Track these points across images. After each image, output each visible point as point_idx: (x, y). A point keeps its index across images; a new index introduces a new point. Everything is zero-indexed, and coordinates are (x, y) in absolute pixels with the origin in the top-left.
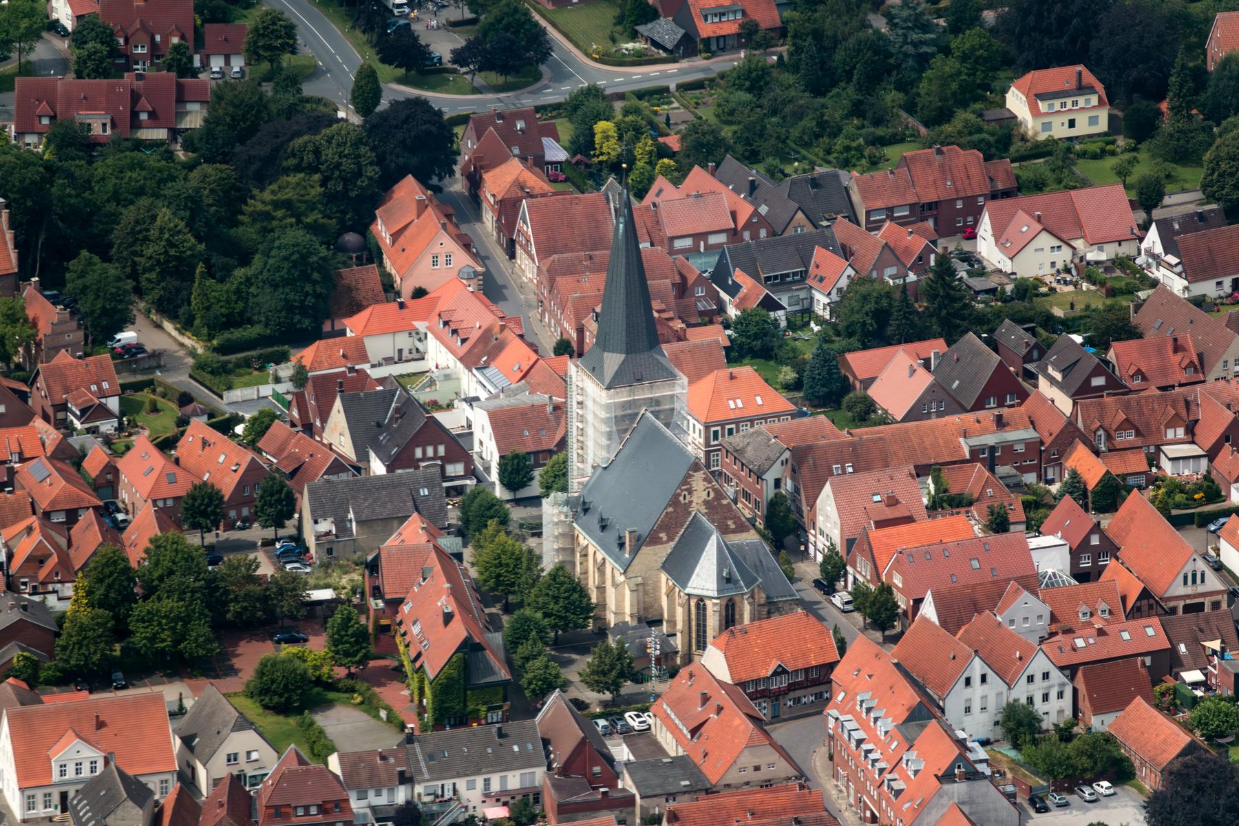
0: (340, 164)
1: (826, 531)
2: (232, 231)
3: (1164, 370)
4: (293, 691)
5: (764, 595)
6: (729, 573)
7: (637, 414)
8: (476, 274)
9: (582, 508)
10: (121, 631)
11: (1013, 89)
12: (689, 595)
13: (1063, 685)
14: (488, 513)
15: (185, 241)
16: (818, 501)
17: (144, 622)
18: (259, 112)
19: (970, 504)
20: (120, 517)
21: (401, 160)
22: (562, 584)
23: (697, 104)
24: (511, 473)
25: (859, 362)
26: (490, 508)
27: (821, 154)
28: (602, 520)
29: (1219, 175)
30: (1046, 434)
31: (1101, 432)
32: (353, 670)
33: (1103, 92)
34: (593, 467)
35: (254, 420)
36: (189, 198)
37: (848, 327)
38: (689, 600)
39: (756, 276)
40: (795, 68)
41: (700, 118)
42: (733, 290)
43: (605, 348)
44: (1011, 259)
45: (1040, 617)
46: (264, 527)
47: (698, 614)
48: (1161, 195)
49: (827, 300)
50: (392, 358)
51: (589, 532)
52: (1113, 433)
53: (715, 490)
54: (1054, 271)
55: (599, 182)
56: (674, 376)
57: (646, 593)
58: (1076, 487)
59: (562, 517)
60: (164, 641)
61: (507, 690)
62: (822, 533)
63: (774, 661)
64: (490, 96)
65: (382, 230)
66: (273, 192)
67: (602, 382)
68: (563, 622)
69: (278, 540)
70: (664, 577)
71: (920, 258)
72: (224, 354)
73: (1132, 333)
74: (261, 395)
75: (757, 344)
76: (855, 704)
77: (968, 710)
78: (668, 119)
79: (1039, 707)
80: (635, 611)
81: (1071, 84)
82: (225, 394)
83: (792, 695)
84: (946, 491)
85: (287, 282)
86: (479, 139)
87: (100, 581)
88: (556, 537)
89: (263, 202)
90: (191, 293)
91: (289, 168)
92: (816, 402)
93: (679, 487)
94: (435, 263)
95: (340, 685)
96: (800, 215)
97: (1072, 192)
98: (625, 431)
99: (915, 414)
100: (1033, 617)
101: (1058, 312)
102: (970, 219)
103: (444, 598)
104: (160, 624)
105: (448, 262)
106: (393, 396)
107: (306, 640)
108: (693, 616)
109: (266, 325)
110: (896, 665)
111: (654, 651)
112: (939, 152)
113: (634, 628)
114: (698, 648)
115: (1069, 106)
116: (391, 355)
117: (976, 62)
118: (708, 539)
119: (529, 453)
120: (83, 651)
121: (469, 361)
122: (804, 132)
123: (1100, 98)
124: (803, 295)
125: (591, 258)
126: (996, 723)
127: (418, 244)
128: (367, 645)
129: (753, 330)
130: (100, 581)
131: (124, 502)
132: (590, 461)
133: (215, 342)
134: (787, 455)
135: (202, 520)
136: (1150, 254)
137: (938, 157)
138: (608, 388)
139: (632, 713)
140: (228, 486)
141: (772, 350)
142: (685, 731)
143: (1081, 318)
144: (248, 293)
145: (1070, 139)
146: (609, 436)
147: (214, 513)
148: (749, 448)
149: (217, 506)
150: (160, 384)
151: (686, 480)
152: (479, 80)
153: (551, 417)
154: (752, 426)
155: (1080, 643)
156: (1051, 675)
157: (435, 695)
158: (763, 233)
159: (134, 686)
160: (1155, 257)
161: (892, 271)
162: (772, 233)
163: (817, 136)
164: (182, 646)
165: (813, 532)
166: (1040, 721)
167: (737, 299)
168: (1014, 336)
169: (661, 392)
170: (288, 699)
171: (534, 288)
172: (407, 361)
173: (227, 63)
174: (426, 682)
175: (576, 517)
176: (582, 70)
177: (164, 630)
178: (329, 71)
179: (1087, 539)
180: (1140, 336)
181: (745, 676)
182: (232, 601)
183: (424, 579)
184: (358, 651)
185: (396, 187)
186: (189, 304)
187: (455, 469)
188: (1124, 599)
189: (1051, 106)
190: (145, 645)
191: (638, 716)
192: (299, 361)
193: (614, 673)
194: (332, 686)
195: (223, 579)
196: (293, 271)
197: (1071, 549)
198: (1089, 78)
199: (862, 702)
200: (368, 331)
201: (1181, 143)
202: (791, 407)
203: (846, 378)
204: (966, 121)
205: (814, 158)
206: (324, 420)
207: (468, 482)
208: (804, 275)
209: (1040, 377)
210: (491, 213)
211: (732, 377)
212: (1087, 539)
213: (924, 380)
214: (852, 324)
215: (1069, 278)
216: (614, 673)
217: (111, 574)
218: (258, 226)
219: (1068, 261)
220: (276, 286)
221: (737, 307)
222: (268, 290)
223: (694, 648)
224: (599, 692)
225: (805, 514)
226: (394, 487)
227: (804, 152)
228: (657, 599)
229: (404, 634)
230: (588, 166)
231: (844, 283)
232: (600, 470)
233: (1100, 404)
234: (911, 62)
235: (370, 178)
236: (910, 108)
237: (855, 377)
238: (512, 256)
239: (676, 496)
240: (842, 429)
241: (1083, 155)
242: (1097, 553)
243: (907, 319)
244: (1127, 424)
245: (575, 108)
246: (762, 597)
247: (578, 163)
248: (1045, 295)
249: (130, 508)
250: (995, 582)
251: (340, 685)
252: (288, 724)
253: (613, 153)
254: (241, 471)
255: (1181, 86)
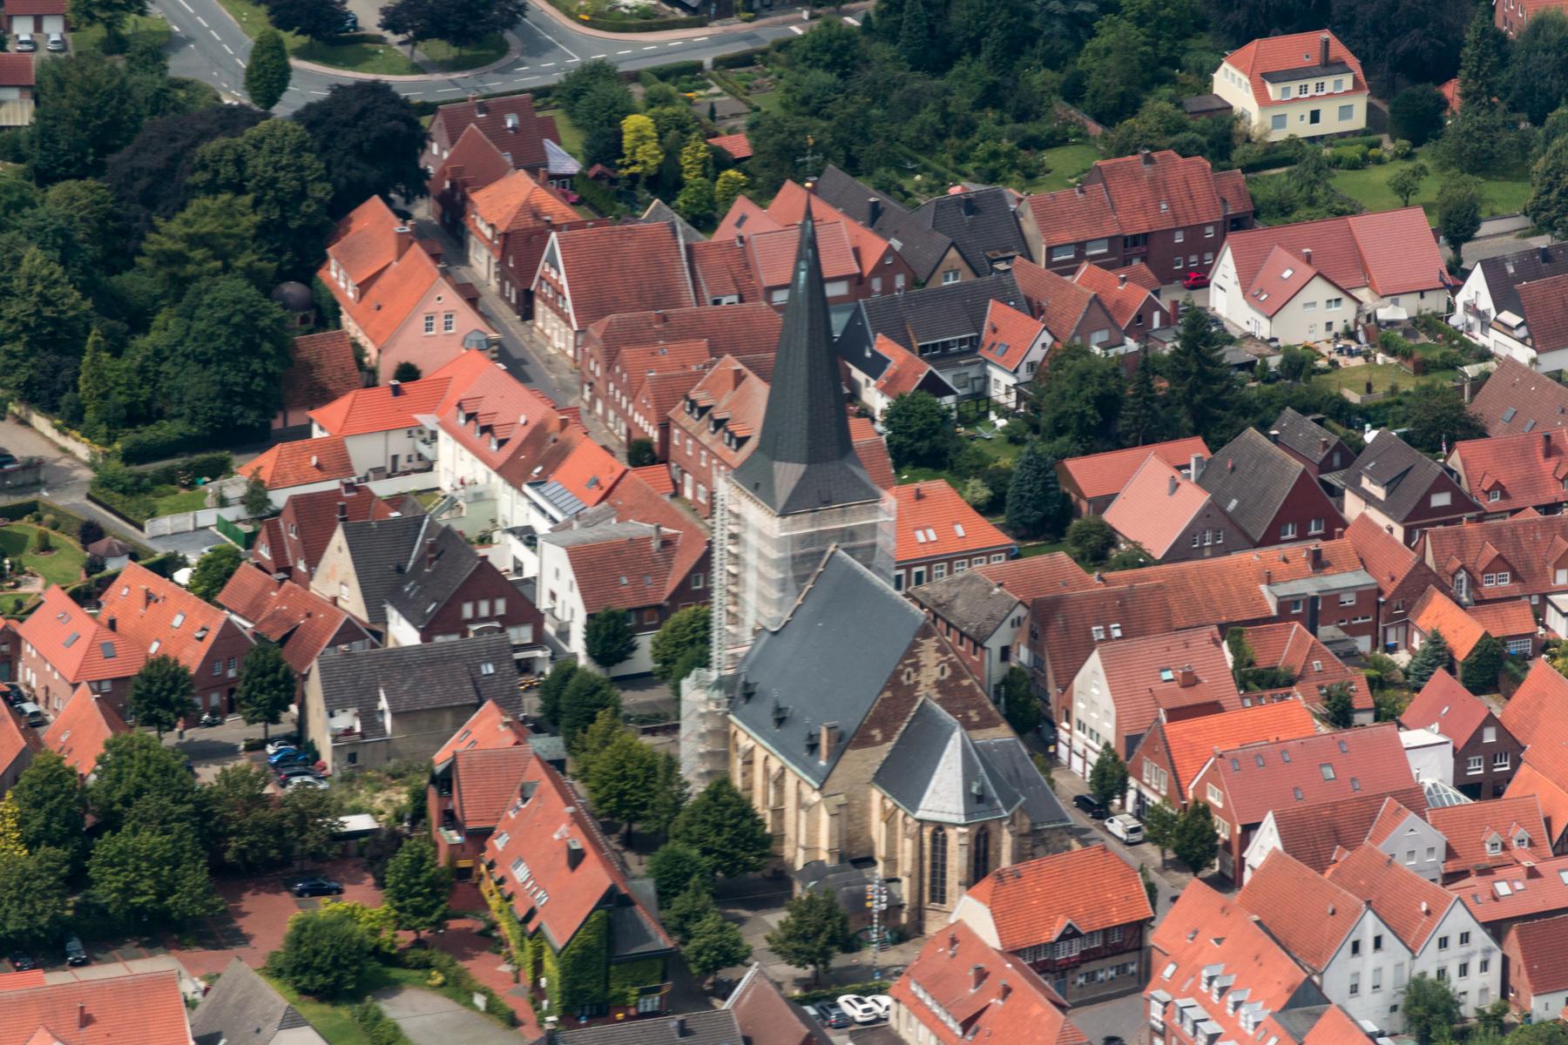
0: (275, 180)
1: (1089, 725)
2: (115, 279)
3: (1531, 483)
4: (346, 967)
5: (1027, 821)
6: (982, 788)
7: (823, 553)
8: (490, 343)
9: (740, 692)
10: (77, 879)
11: (1225, 65)
12: (922, 822)
13: (1488, 951)
14: (592, 701)
15: (65, 296)
16: (1077, 681)
17: (112, 865)
18: (122, 102)
19: (1291, 682)
20: (29, 707)
21: (354, 174)
22: (727, 805)
23: (748, 87)
24: (606, 640)
25: (1087, 473)
26: (592, 693)
27: (951, 163)
28: (779, 710)
29: (1561, 194)
30: (1386, 578)
31: (1463, 575)
32: (423, 934)
33: (1359, 71)
34: (755, 632)
35: (205, 565)
36: (59, 232)
37: (1057, 420)
38: (921, 828)
39: (907, 345)
40: (892, 36)
41: (757, 109)
42: (875, 367)
43: (775, 456)
44: (1270, 318)
45: (1431, 850)
46: (251, 722)
47: (934, 849)
48: (1476, 224)
49: (1012, 381)
50: (382, 469)
51: (756, 727)
52: (1479, 577)
53: (953, 666)
54: (1330, 335)
55: (636, 205)
56: (876, 497)
57: (850, 818)
58: (1438, 655)
59: (712, 707)
60: (144, 893)
61: (669, 962)
62: (1081, 726)
63: (1061, 918)
64: (438, 77)
65: (337, 277)
66: (187, 223)
67: (772, 504)
68: (733, 865)
69: (272, 741)
70: (876, 795)
71: (1139, 318)
72: (140, 463)
73: (1474, 430)
74: (200, 524)
75: (924, 445)
76: (1198, 982)
77: (1354, 989)
78: (713, 111)
79: (1456, 984)
80: (835, 845)
81: (1313, 60)
82: (148, 524)
83: (1085, 968)
84: (1251, 663)
85: (223, 356)
86: (453, 141)
87: (38, 805)
88: (702, 736)
89: (171, 237)
90: (78, 374)
91: (195, 187)
92: (1023, 532)
93: (901, 662)
94: (429, 327)
95: (409, 958)
96: (953, 253)
97: (1351, 219)
98: (805, 578)
99: (1181, 551)
100: (1421, 850)
101: (1354, 397)
102: (1193, 258)
103: (563, 828)
104: (137, 869)
105: (448, 326)
106: (420, 526)
107: (340, 891)
108: (927, 853)
109: (192, 421)
110: (1258, 923)
111: (877, 904)
112: (1149, 160)
113: (834, 870)
114: (933, 899)
115: (1312, 91)
116: (381, 465)
117: (1159, 26)
118: (947, 738)
119: (630, 610)
120: (26, 909)
121: (513, 473)
122: (921, 131)
123: (1355, 80)
124: (973, 372)
125: (665, 319)
126: (1394, 1008)
127: (386, 291)
128: (443, 903)
129: (917, 425)
130: (38, 805)
131: (28, 686)
132: (750, 620)
133: (117, 446)
134: (1021, 611)
135: (162, 713)
136: (1471, 308)
137: (1148, 168)
138: (783, 515)
139: (851, 997)
140: (192, 658)
141: (945, 454)
142: (952, 1025)
143: (1388, 405)
144: (157, 373)
145: (1312, 139)
146: (783, 586)
147: (180, 702)
148: (959, 602)
149: (184, 692)
150: (49, 509)
151: (912, 651)
152: (420, 53)
153: (659, 557)
154: (950, 572)
155: (1503, 889)
156: (1472, 937)
157: (564, 973)
158: (900, 281)
159: (99, 961)
160: (1481, 315)
161: (1100, 336)
162: (913, 282)
163: (941, 136)
164: (170, 900)
165: (1066, 725)
166: (1458, 1004)
167: (883, 379)
168: (1314, 435)
169: (857, 520)
170: (339, 979)
171: (569, 364)
172: (406, 473)
173: (38, 28)
174: (547, 953)
175: (732, 706)
176: (566, 38)
177: (142, 877)
178: (190, 40)
179: (1478, 734)
180: (1486, 436)
181: (1021, 942)
182: (233, 833)
183: (525, 800)
184: (434, 907)
185: (352, 214)
186: (76, 389)
187: (522, 634)
188: (1548, 821)
189: (1286, 91)
190: (115, 900)
191: (861, 1002)
192: (255, 473)
193: (823, 938)
194: (393, 959)
195: (218, 801)
196: (234, 340)
197: (1455, 749)
198: (1339, 50)
199: (1211, 979)
200: (350, 428)
201: (1485, 144)
202: (1005, 540)
203: (1067, 497)
204: (1162, 113)
205: (942, 169)
206: (313, 560)
207: (539, 653)
208: (975, 344)
209: (1347, 493)
210: (485, 252)
211: (919, 496)
212: (1478, 734)
213: (1194, 499)
214: (1064, 415)
215: (1354, 346)
216: (823, 938)
217: (56, 794)
218: (161, 273)
219: (1351, 322)
220: (206, 363)
221: (884, 390)
222: (193, 367)
223: (927, 899)
224: (799, 965)
225: (1052, 698)
226: (446, 662)
227: (924, 160)
228: (865, 827)
229: (501, 882)
230: (613, 181)
231: (1037, 354)
232: (766, 636)
233: (1458, 533)
234: (1059, 26)
235: (319, 201)
236: (1073, 92)
237: (1081, 495)
238: (527, 313)
239: (897, 674)
240: (1090, 571)
241: (1337, 162)
242: (1492, 754)
243: (1148, 408)
244: (1500, 564)
245: (576, 96)
246: (1025, 824)
247: (598, 177)
248: (1325, 371)
249: (41, 695)
250: (1360, 800)
251: (409, 958)
252: (339, 1016)
253: (652, 162)
254: (211, 638)
255: (1481, 60)
